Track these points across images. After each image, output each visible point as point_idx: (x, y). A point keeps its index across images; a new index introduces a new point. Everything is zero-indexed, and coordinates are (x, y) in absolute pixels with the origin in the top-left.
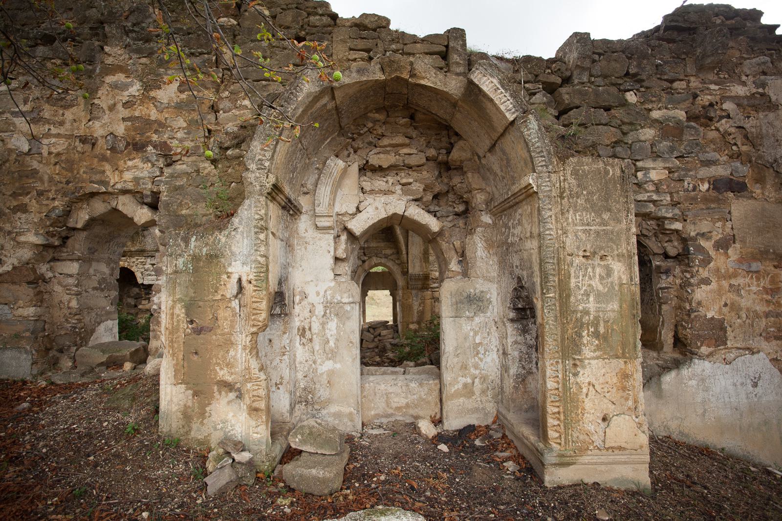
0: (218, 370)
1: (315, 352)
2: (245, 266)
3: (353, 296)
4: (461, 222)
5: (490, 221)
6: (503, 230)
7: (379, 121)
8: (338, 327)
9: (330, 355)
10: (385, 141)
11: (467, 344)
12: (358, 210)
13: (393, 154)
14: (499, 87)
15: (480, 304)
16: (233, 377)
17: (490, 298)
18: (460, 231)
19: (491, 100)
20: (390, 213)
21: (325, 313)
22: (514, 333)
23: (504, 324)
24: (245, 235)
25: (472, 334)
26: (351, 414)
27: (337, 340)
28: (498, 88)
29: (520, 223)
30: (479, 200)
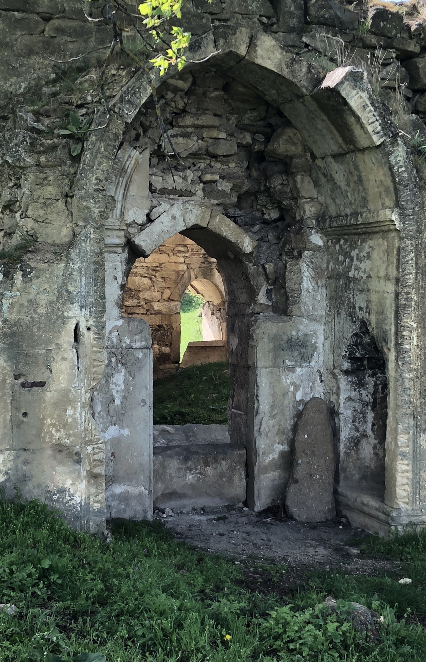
0: (54, 432)
1: (96, 415)
2: (83, 310)
3: (146, 340)
4: (271, 234)
5: (321, 243)
6: (341, 258)
7: (181, 90)
8: (125, 382)
9: (114, 419)
10: (189, 121)
11: (286, 403)
12: (150, 220)
13: (195, 138)
14: (368, 103)
15: (303, 350)
16: (71, 439)
17: (316, 343)
18: (269, 248)
19: (358, 118)
20: (190, 225)
21: (110, 361)
22: (348, 387)
23: (335, 376)
24: (83, 273)
25: (292, 389)
26: (140, 494)
27: (125, 398)
28: (367, 105)
29: (369, 256)
30: (307, 213)
